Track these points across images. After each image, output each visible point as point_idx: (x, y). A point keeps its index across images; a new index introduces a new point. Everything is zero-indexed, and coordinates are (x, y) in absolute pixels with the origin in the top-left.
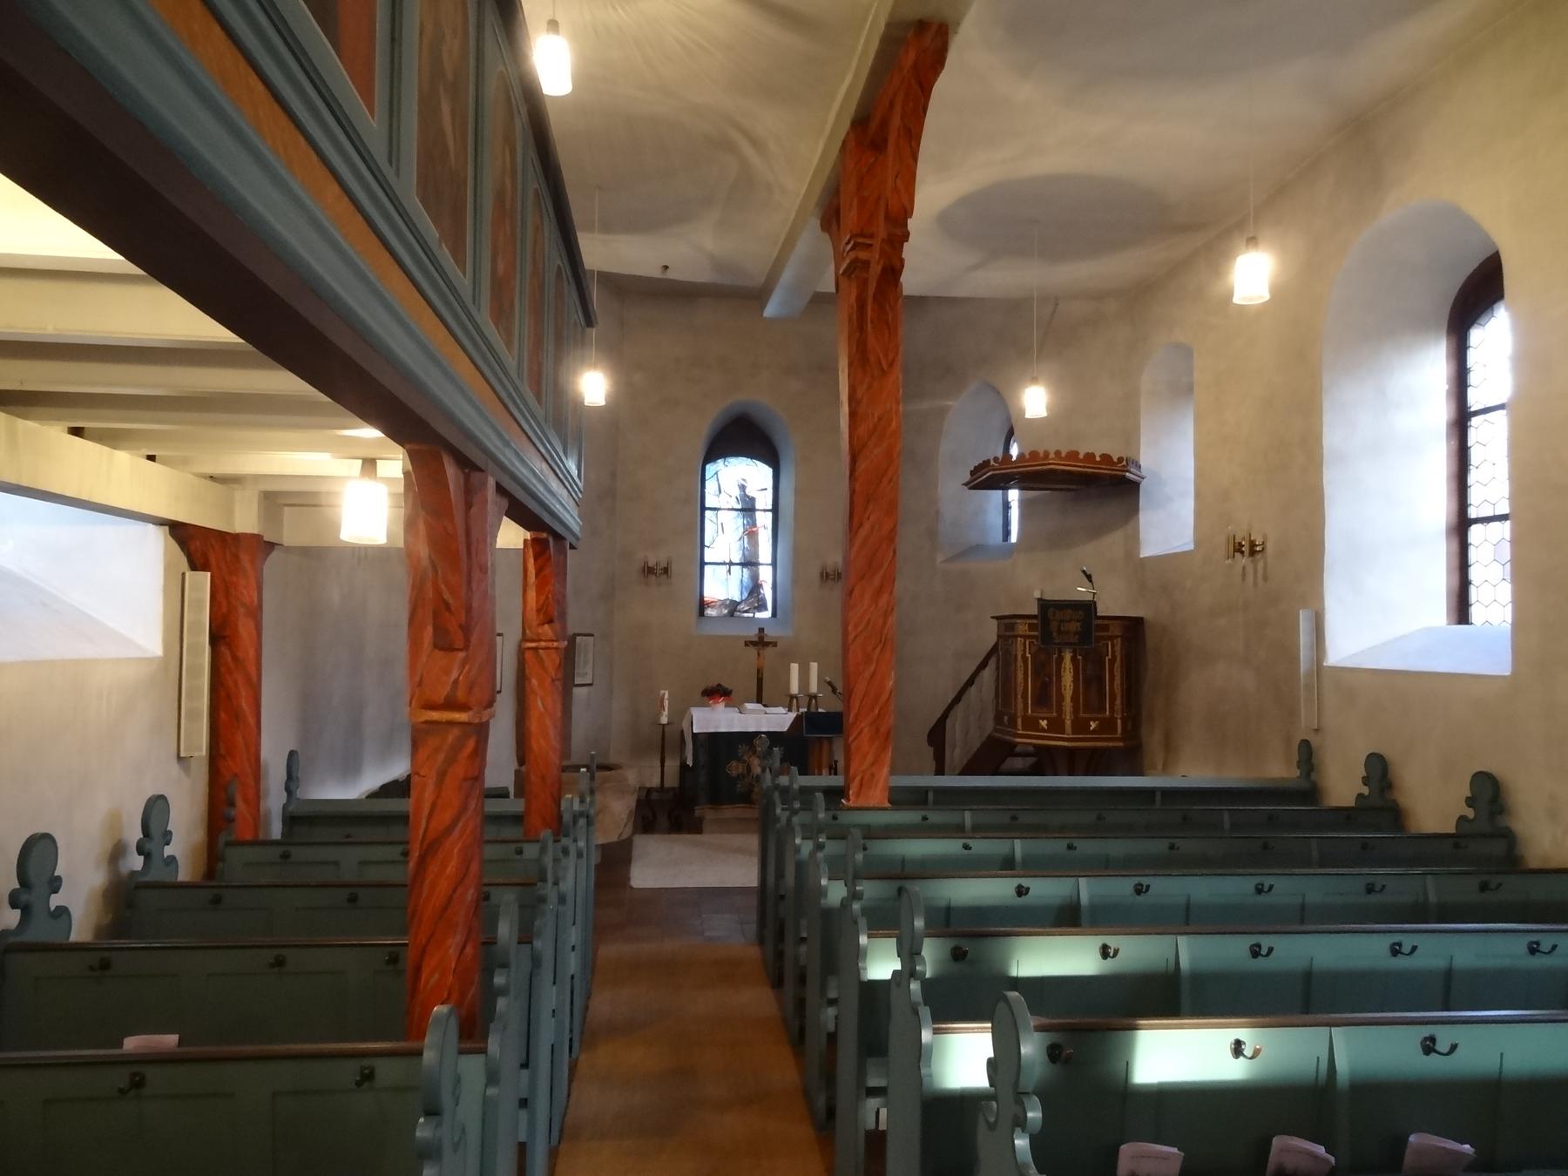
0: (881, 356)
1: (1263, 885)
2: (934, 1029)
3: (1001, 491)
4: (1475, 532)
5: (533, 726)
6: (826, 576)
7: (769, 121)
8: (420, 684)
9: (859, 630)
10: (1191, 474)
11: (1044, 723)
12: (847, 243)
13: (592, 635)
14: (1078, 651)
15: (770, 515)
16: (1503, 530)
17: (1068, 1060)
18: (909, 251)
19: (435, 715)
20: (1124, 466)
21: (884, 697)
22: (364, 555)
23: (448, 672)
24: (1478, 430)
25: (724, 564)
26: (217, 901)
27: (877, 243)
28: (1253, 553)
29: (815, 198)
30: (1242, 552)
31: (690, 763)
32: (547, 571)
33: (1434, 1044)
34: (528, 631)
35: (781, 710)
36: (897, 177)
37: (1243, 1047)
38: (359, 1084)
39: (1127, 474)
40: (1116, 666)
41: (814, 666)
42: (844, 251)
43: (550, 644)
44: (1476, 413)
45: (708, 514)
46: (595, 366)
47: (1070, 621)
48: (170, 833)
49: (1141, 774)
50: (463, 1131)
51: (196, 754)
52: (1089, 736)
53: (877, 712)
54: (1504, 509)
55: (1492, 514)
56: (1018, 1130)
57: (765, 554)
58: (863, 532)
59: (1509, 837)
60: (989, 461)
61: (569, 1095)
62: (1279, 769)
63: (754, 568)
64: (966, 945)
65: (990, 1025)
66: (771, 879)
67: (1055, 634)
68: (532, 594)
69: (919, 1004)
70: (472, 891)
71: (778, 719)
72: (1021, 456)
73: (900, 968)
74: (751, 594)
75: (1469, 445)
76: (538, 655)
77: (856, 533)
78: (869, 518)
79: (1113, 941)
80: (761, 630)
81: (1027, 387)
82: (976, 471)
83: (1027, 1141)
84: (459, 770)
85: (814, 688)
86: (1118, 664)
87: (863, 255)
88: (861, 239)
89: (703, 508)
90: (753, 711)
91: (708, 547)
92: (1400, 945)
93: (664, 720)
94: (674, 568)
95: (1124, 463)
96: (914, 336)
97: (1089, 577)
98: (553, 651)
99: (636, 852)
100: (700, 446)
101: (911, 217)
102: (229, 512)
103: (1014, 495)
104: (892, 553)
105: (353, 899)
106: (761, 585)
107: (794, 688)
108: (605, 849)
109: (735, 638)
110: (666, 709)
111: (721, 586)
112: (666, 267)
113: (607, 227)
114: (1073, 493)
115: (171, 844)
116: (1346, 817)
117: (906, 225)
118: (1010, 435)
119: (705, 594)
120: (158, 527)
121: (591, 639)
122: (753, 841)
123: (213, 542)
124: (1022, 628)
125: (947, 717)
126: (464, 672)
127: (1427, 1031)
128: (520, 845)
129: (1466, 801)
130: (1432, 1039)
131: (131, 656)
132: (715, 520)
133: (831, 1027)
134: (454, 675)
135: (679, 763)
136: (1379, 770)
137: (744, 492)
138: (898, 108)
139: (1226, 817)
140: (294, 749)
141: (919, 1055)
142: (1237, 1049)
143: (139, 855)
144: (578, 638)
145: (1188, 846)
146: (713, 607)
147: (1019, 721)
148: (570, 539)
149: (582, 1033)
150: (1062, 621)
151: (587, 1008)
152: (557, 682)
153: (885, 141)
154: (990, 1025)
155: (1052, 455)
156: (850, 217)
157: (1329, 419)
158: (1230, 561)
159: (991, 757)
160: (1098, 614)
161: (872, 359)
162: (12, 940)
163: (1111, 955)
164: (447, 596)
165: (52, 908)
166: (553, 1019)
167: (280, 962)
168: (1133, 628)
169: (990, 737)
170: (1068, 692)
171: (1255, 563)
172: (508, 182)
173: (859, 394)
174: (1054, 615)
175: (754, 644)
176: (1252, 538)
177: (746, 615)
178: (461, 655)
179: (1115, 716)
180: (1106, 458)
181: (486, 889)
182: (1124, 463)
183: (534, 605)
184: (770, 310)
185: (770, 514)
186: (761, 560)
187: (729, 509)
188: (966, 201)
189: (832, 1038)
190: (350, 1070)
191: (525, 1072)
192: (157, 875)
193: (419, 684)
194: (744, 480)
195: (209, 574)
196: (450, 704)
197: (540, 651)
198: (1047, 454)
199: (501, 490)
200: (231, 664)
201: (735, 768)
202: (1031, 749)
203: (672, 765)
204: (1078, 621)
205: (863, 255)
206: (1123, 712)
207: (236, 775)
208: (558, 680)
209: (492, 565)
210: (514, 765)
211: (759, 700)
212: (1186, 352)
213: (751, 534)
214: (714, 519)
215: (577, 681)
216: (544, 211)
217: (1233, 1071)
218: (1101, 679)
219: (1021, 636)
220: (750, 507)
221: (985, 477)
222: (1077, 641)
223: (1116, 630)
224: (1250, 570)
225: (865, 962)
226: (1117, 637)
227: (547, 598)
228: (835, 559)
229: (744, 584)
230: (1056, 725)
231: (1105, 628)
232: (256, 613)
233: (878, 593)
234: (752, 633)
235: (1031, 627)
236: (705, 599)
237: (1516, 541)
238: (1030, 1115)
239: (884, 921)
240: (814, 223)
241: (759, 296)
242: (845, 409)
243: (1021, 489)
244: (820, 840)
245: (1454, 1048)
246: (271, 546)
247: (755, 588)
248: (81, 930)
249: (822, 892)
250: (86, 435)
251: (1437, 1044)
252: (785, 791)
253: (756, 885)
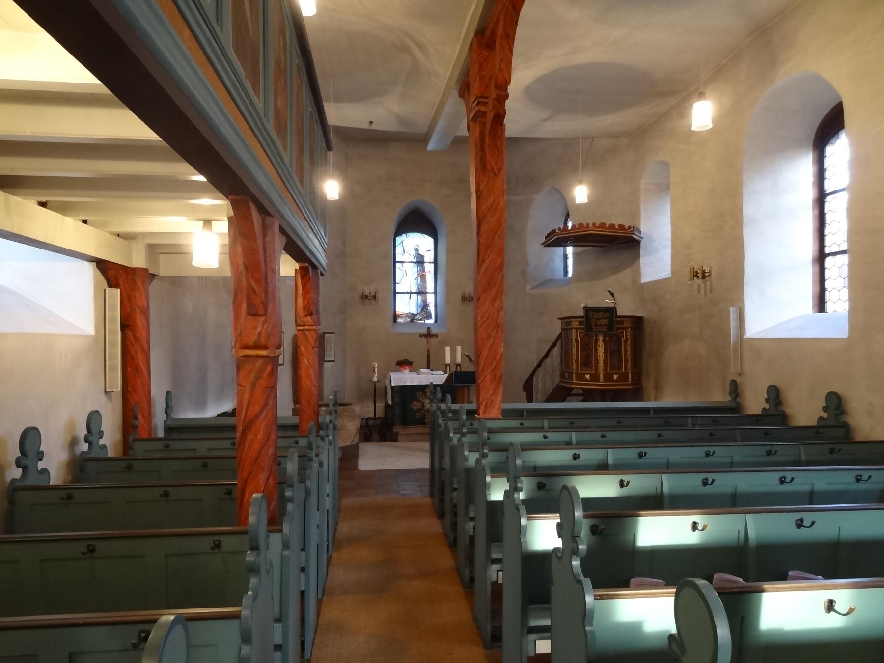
0: (494, 165)
1: (709, 452)
2: (528, 517)
3: (562, 248)
4: (828, 261)
5: (303, 373)
6: (465, 299)
7: (429, 33)
8: (240, 335)
9: (484, 320)
10: (669, 235)
11: (588, 376)
12: (474, 102)
13: (333, 333)
14: (606, 336)
15: (432, 265)
16: (844, 259)
17: (601, 533)
18: (508, 103)
19: (249, 352)
20: (632, 231)
21: (498, 357)
22: (207, 281)
23: (255, 328)
24: (830, 204)
25: (407, 293)
26: (129, 467)
27: (490, 101)
28: (704, 277)
29: (455, 77)
30: (698, 277)
31: (390, 402)
32: (309, 285)
33: (802, 523)
34: (298, 320)
35: (441, 372)
36: (501, 62)
37: (698, 525)
38: (213, 549)
39: (634, 236)
40: (628, 343)
41: (459, 348)
42: (472, 106)
43: (311, 327)
44: (829, 194)
45: (398, 265)
46: (332, 177)
47: (602, 318)
48: (102, 431)
49: (642, 400)
50: (271, 565)
51: (115, 390)
53: (494, 366)
54: (844, 247)
55: (837, 250)
56: (574, 557)
57: (430, 287)
58: (485, 266)
59: (846, 427)
60: (555, 230)
61: (327, 574)
62: (719, 396)
63: (424, 295)
64: (544, 480)
65: (559, 515)
66: (437, 465)
67: (593, 326)
68: (300, 299)
69: (519, 505)
70: (271, 449)
71: (439, 377)
72: (573, 226)
73: (509, 489)
74: (422, 310)
75: (825, 213)
76: (304, 335)
77: (481, 266)
78: (488, 257)
79: (626, 478)
80: (429, 328)
81: (576, 186)
82: (548, 236)
83: (579, 562)
84: (263, 382)
85: (459, 360)
86: (629, 343)
87: (482, 108)
88: (482, 99)
89: (395, 262)
90: (424, 373)
91: (398, 284)
92: (785, 478)
93: (375, 379)
94: (379, 296)
95: (632, 229)
96: (513, 161)
97: (612, 294)
98: (313, 331)
99: (361, 451)
100: (392, 226)
101: (509, 85)
102: (129, 255)
103: (570, 250)
104: (501, 277)
105: (205, 466)
106: (428, 305)
107: (448, 361)
108: (343, 449)
109: (415, 334)
110: (376, 373)
111: (406, 305)
112: (371, 122)
113: (338, 99)
114: (603, 248)
115: (103, 438)
116: (755, 419)
117: (506, 90)
118: (567, 216)
119: (397, 310)
120: (90, 263)
121: (333, 336)
122: (426, 445)
123: (121, 271)
124: (575, 323)
125: (534, 375)
126: (264, 328)
127: (798, 515)
128: (296, 439)
129: (823, 409)
130: (802, 520)
131: (78, 334)
132: (401, 268)
133: (471, 532)
134: (259, 330)
135: (384, 405)
136: (775, 395)
137: (418, 252)
138: (501, 23)
139: (689, 421)
140: (169, 390)
141: (519, 532)
142: (695, 526)
143: (86, 443)
144: (326, 335)
145: (667, 434)
146: (401, 317)
147: (574, 375)
148: (321, 269)
149: (333, 542)
150: (598, 319)
151: (335, 531)
152: (315, 348)
153: (494, 42)
154: (559, 515)
155: (591, 225)
156: (475, 88)
157: (746, 199)
158: (691, 282)
159: (561, 393)
160: (618, 315)
161: (489, 167)
162: (18, 484)
163: (625, 485)
164: (254, 285)
165: (39, 469)
166: (318, 512)
167: (166, 495)
168: (637, 322)
169: (558, 386)
170: (601, 359)
171: (705, 283)
172: (282, 56)
173: (482, 187)
174: (593, 316)
175: (425, 336)
176: (704, 269)
177: (420, 321)
178: (262, 318)
179: (628, 372)
180: (622, 227)
181: (279, 459)
182: (632, 229)
183: (302, 306)
184: (431, 146)
185: (433, 265)
186: (428, 291)
187: (409, 262)
188: (540, 80)
189: (472, 540)
190: (208, 541)
191: (303, 553)
192: (96, 454)
193: (239, 335)
194: (418, 246)
195: (119, 290)
196: (257, 346)
197: (305, 331)
198: (588, 225)
199: (282, 231)
200: (133, 341)
201: (415, 405)
202: (581, 392)
203: (380, 405)
204: (606, 318)
205: (482, 108)
206: (632, 370)
207: (137, 402)
208: (316, 347)
209: (278, 269)
210: (292, 406)
211: (428, 368)
212: (665, 165)
213: (422, 276)
214: (401, 268)
215: (326, 359)
216: (302, 78)
217: (692, 538)
218: (620, 351)
219: (575, 328)
220: (421, 261)
221: (553, 239)
222: (606, 330)
223: (627, 324)
224: (702, 286)
225: (489, 491)
226: (628, 327)
227: (309, 300)
228: (469, 289)
229: (419, 304)
230: (595, 377)
231: (622, 322)
232: (146, 312)
233: (494, 299)
234: (424, 331)
235: (581, 323)
236: (397, 313)
237: (851, 266)
238: (580, 547)
239: (498, 471)
240: (455, 93)
241: (424, 139)
242: (474, 196)
243: (574, 246)
244: (464, 430)
245: (813, 523)
246: (153, 276)
247: (425, 306)
248: (56, 477)
249: (466, 459)
250: (48, 207)
251: (804, 522)
252: (443, 413)
253: (428, 467)
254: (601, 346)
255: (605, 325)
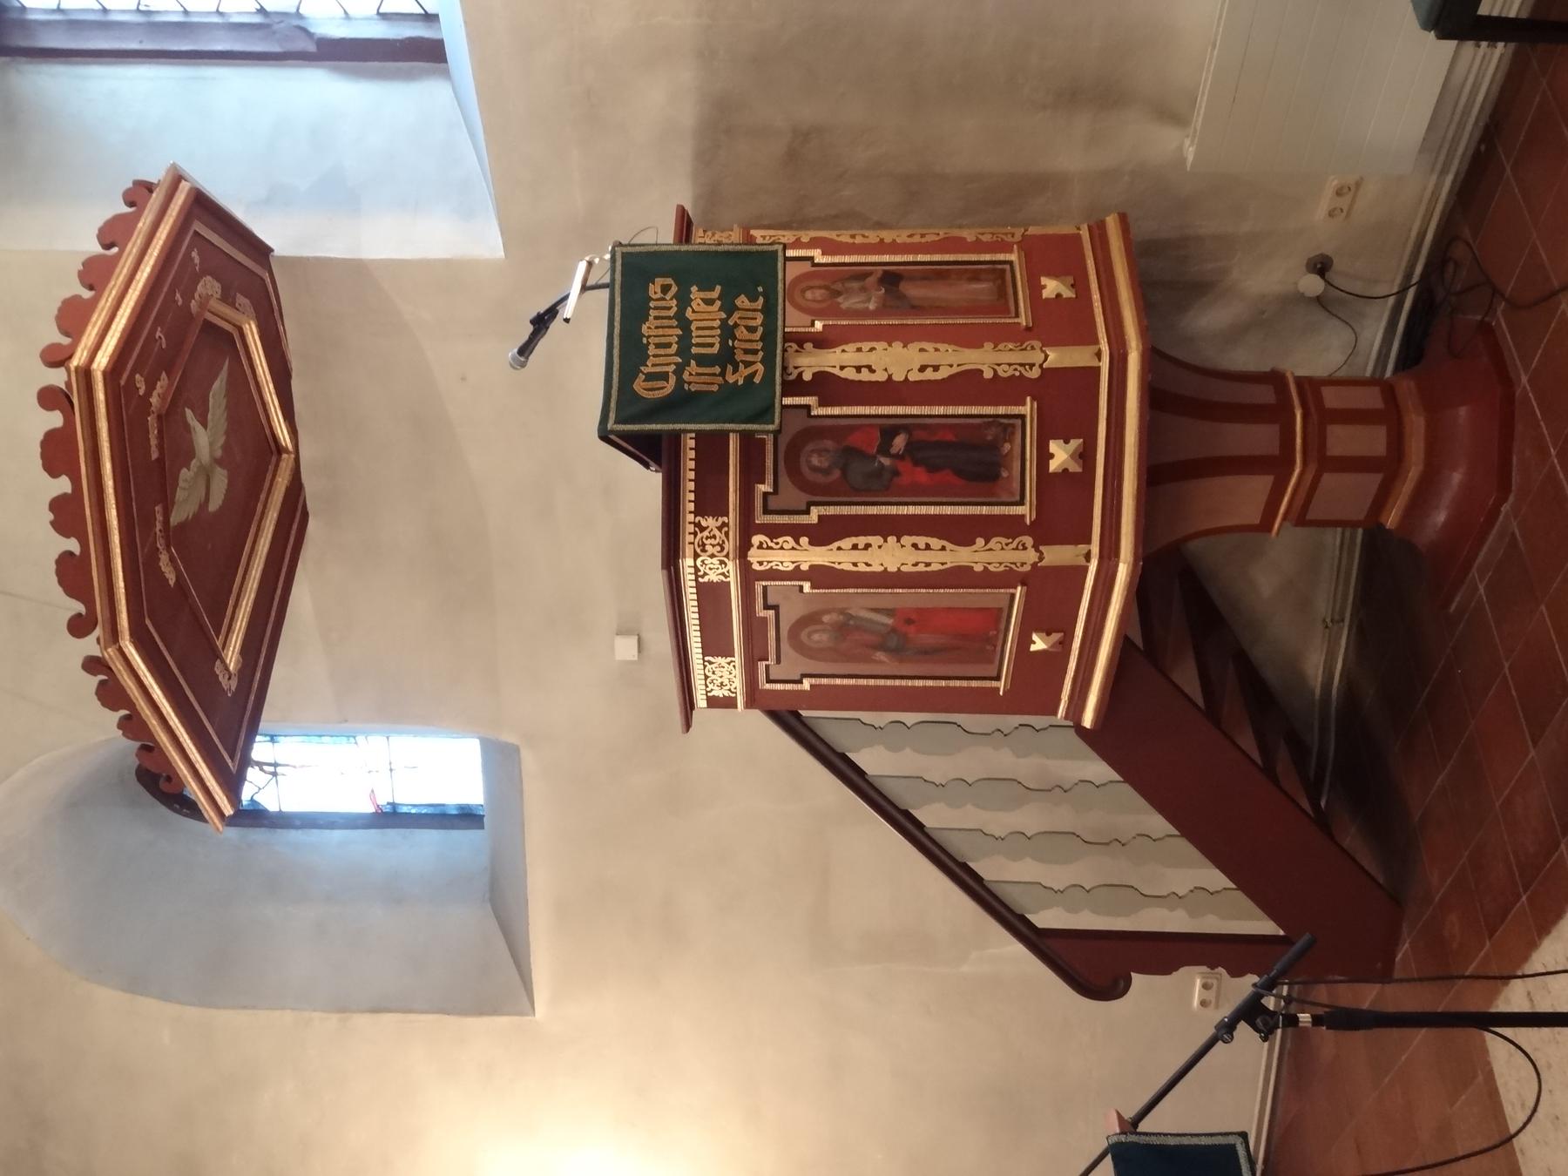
47: (685, 324)
52: (1096, 296)
179: (1035, 373)
204: (684, 300)
254: (863, 359)
255: (729, 308)
